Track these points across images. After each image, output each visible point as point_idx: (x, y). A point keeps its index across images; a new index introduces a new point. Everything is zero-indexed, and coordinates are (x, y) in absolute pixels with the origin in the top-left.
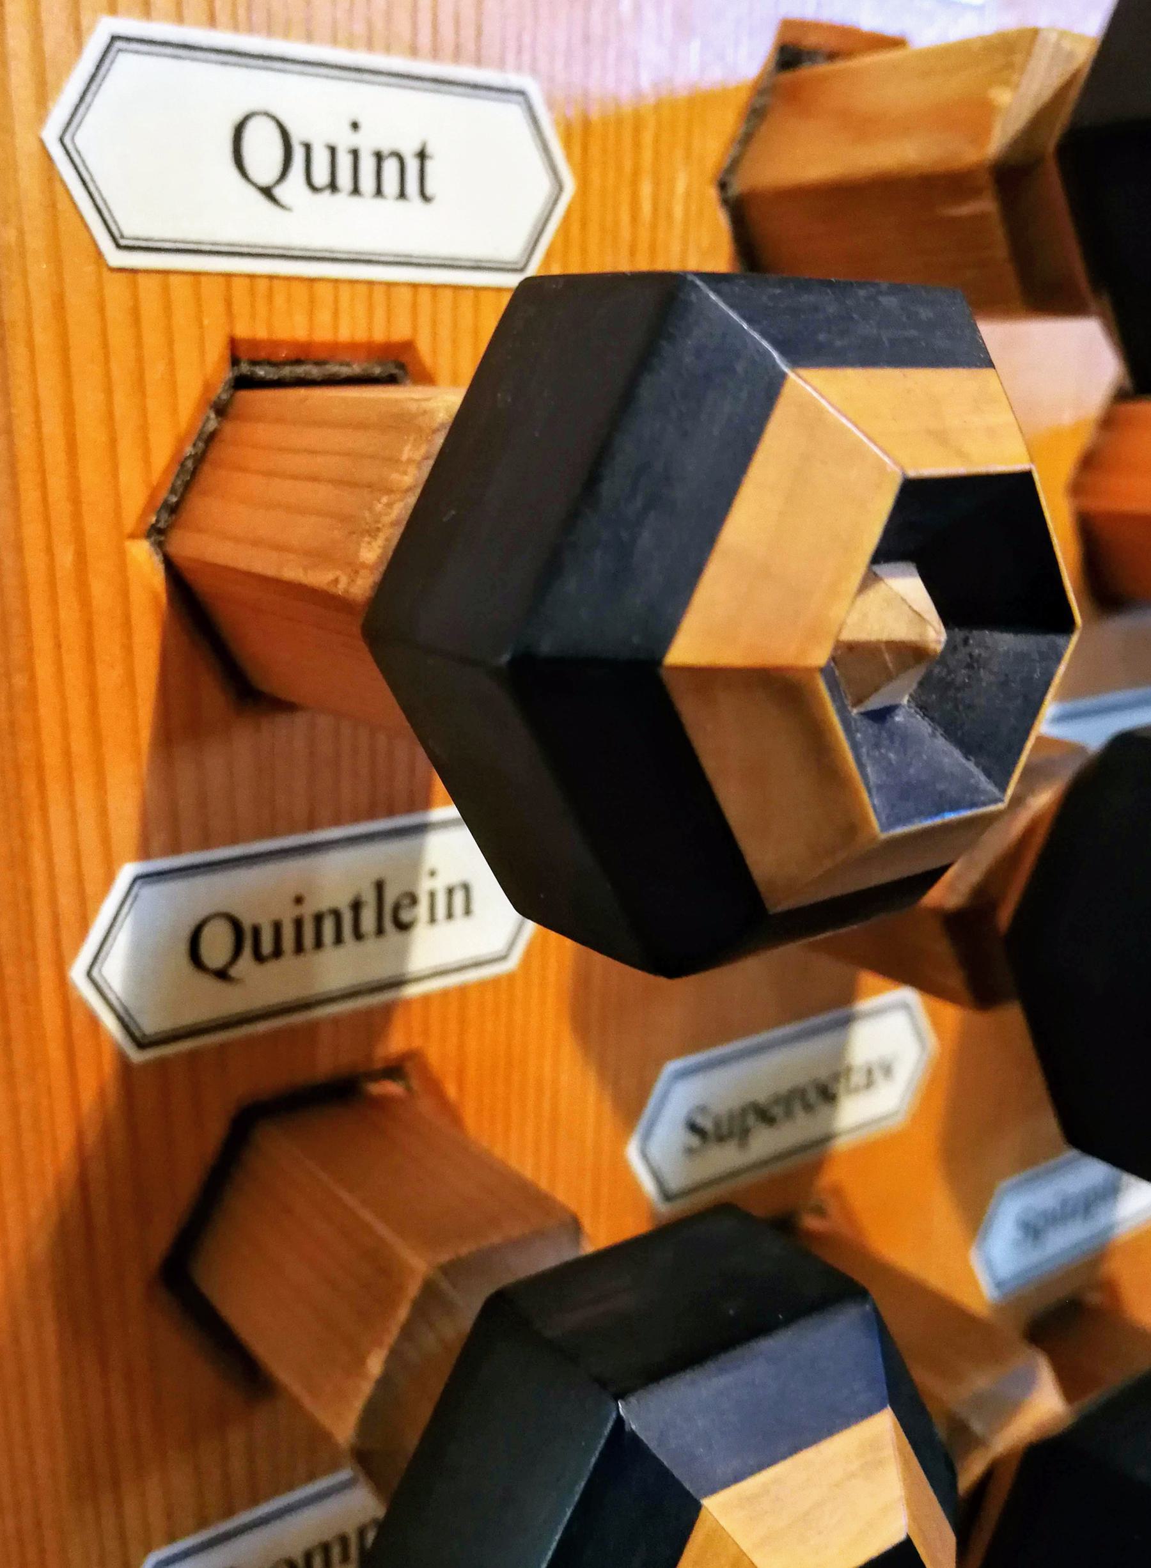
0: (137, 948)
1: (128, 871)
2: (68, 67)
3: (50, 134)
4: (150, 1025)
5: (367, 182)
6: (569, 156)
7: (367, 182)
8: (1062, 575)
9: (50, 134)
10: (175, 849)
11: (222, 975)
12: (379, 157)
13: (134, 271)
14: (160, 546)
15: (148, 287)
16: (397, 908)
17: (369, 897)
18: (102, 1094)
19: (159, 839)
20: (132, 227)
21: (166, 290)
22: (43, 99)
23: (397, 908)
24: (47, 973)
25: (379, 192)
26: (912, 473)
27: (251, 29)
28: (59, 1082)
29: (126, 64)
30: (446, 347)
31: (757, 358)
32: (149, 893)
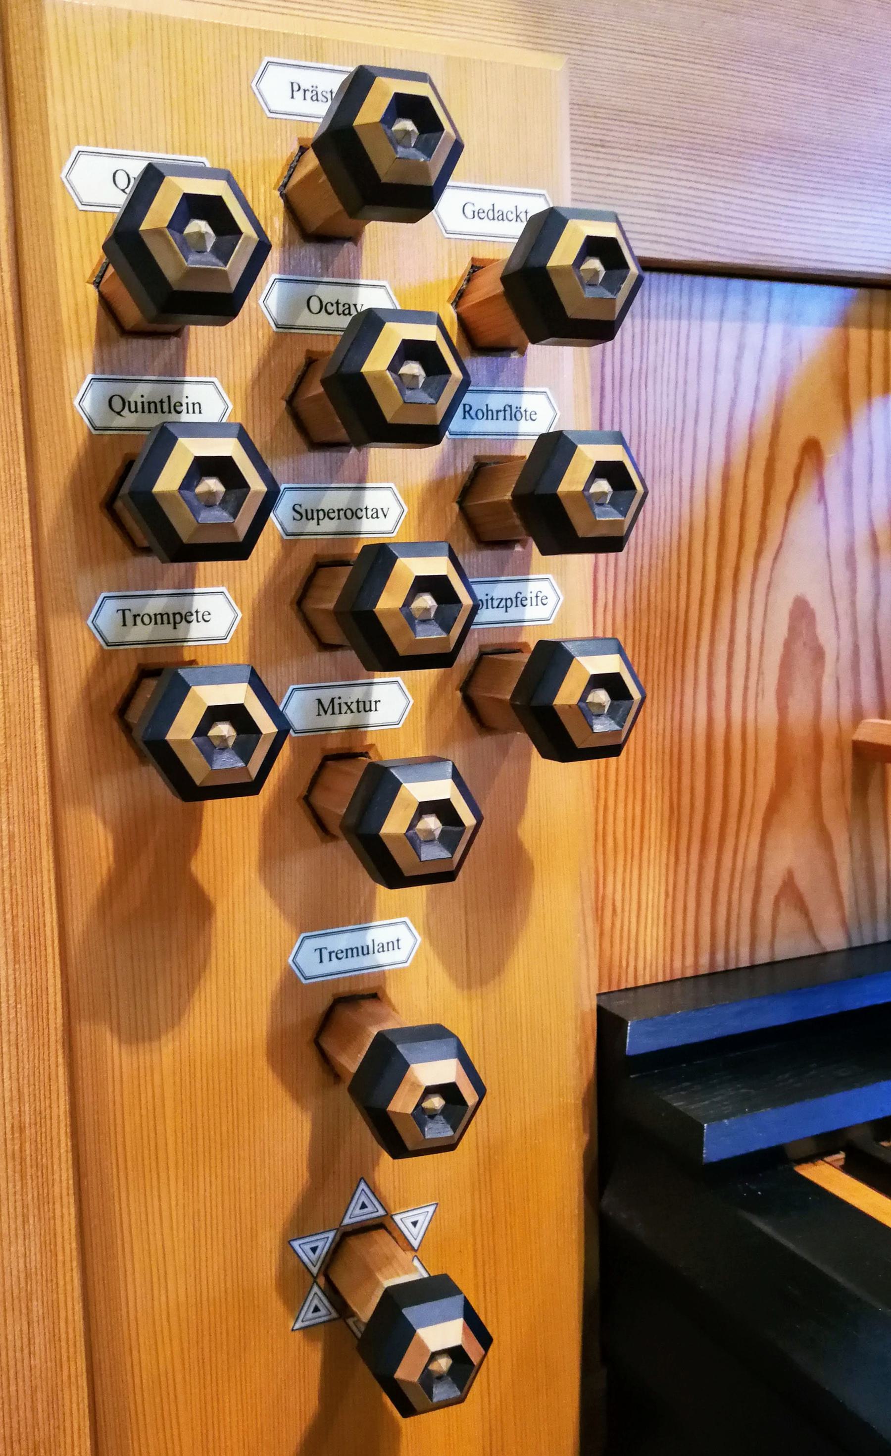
0: (93, 399)
1: (90, 376)
2: (67, 160)
3: (63, 175)
4: (98, 424)
5: (191, 410)
6: (228, 393)
7: (191, 410)
8: (204, 814)
9: (63, 175)
10: (103, 373)
11: (119, 413)
12: (194, 404)
13: (86, 211)
14: (97, 287)
15: (90, 215)
16: (175, 406)
17: (166, 400)
18: (84, 440)
19: (98, 370)
20: (85, 200)
21: (95, 216)
22: (61, 168)
23: (175, 406)
24: (68, 402)
25: (194, 412)
26: (246, 705)
27: (117, 148)
28: (72, 433)
29: (83, 158)
30: (263, 900)
31: (287, 246)
32: (96, 384)
